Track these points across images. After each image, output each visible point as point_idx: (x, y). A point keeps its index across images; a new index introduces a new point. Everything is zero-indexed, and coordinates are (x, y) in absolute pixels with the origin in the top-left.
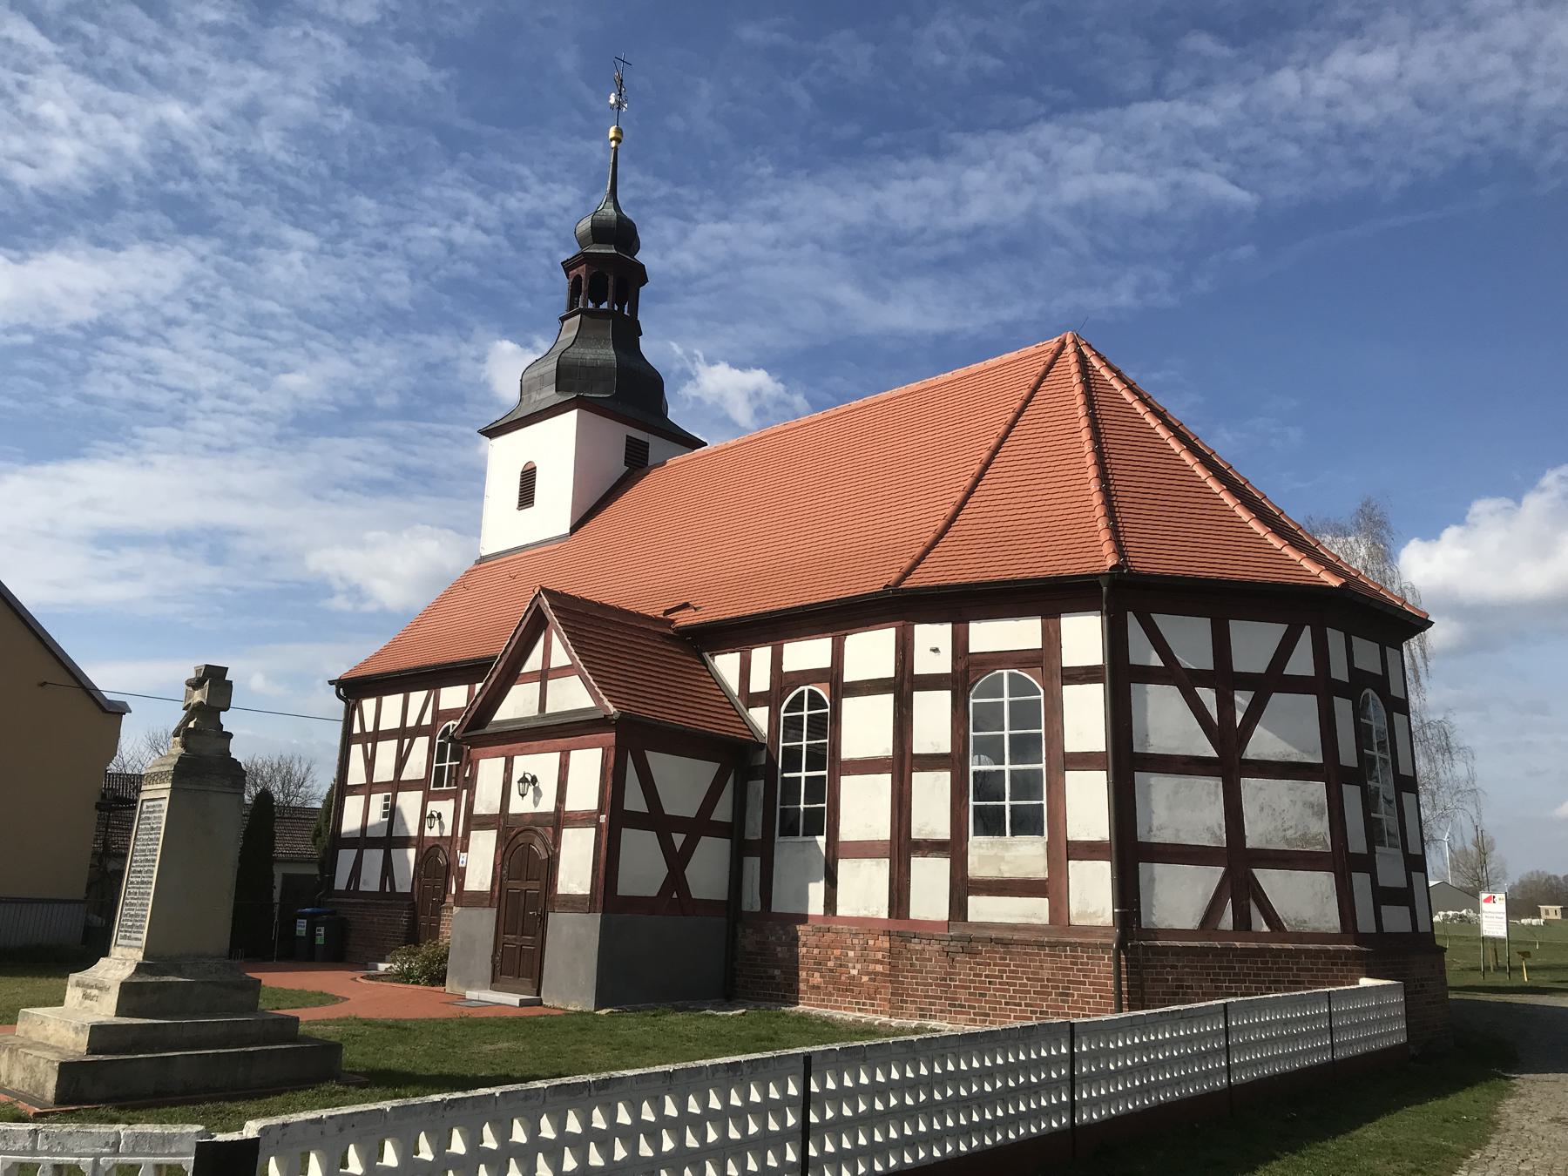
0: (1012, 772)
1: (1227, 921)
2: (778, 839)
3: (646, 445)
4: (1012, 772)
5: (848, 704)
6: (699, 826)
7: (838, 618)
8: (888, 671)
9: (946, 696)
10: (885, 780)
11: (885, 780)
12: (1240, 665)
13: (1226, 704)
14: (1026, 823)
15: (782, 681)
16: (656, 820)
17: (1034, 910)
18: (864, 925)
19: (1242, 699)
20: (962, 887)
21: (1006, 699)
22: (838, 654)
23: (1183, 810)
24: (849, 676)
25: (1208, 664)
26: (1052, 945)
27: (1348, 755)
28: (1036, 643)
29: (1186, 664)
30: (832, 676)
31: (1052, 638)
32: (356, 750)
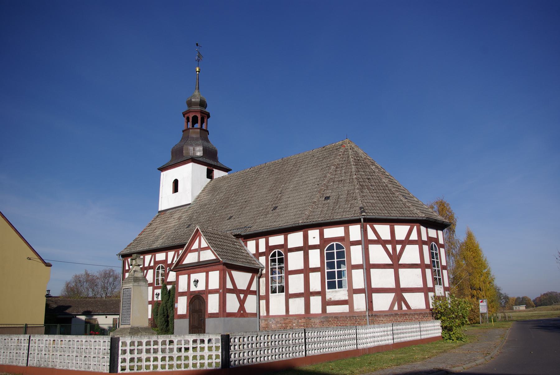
1: (396, 308)
2: (270, 294)
5: (290, 254)
7: (286, 231)
8: (301, 244)
9: (318, 250)
10: (302, 276)
11: (302, 276)
13: (394, 249)
15: (269, 248)
16: (235, 291)
17: (345, 309)
18: (299, 316)
19: (399, 247)
20: (325, 303)
21: (335, 251)
22: (286, 240)
23: (383, 278)
24: (290, 246)
27: (427, 261)
28: (328, 307)
29: (383, 238)
30: (284, 246)
31: (347, 232)
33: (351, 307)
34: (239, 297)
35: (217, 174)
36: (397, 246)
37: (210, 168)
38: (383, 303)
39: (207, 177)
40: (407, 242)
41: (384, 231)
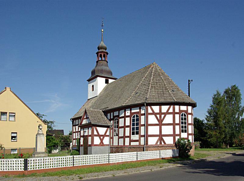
0: (135, 127)
1: (159, 143)
3: (108, 80)
4: (135, 127)
6: (105, 135)
12: (162, 112)
13: (160, 117)
14: (137, 133)
15: (181, 111)
16: (98, 135)
17: (137, 143)
19: (163, 116)
20: (131, 141)
25: (158, 112)
26: (139, 147)
32: (74, 127)
33: (140, 143)
34: (100, 138)
35: (110, 81)
36: (162, 115)
37: (107, 79)
38: (152, 141)
39: (106, 83)
40: (167, 113)
41: (156, 109)
